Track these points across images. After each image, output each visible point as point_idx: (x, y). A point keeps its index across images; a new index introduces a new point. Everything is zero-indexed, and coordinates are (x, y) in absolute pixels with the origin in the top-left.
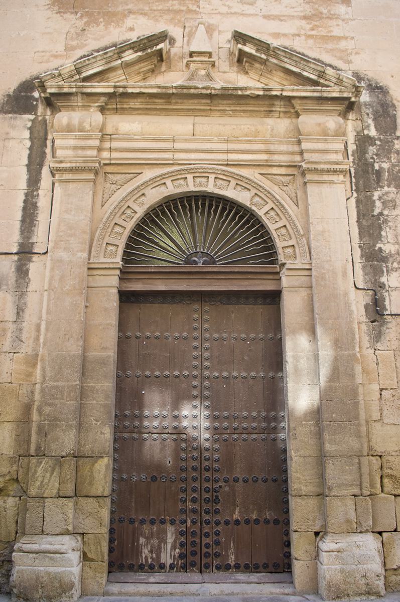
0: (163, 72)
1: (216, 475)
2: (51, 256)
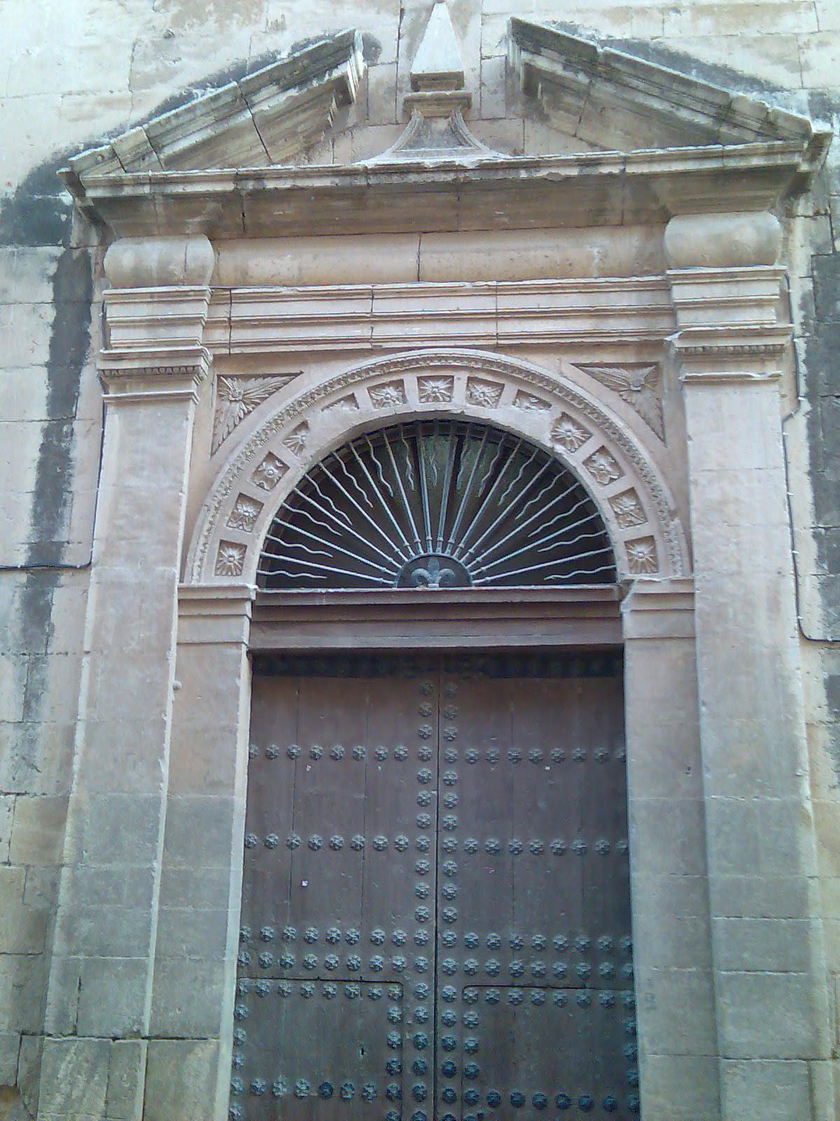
0: (350, 129)
1: (471, 1088)
2: (99, 574)
